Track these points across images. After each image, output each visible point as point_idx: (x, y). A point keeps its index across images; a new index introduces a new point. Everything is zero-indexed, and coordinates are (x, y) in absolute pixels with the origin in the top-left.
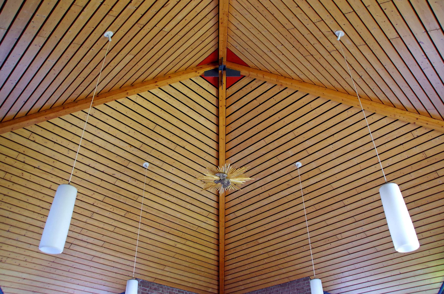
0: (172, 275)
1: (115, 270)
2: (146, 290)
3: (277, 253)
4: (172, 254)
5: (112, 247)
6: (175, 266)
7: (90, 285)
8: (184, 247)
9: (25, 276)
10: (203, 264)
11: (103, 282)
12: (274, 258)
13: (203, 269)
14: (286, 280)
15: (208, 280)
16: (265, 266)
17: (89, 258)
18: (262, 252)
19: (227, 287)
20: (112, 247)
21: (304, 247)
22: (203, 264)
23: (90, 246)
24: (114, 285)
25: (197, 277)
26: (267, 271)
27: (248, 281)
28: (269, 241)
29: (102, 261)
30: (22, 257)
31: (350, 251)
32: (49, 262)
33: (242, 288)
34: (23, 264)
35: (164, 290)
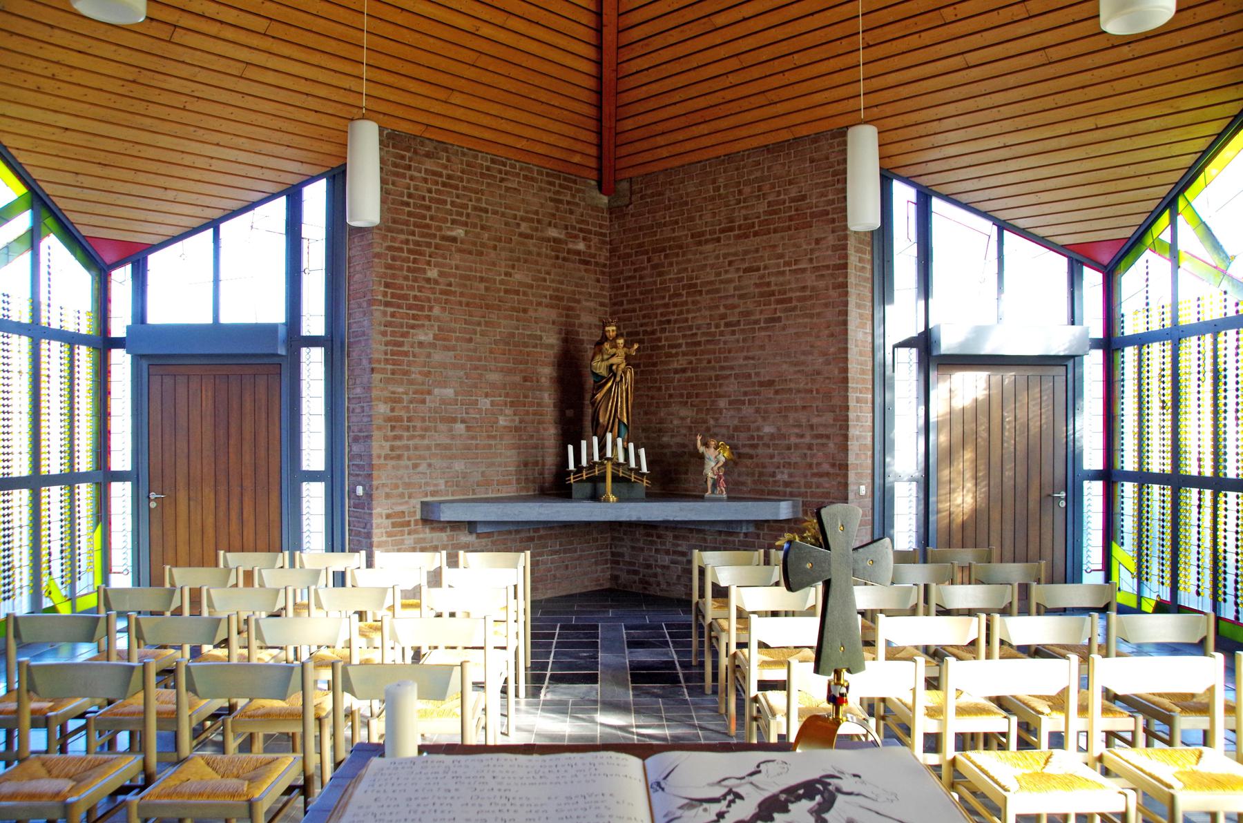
0: (473, 117)
1: (312, 103)
2: (403, 157)
3: (764, 58)
4: (469, 56)
5: (293, 35)
6: (481, 91)
7: (247, 144)
8: (502, 36)
9: (64, 121)
10: (555, 86)
11: (286, 139)
12: (756, 72)
13: (556, 101)
14: (785, 135)
15: (571, 131)
16: (729, 95)
17: (235, 68)
18: (722, 52)
19: (623, 151)
20: (293, 35)
21: (844, 41)
22: (555, 86)
23: (229, 33)
24: (316, 146)
25: (540, 122)
26: (735, 107)
27: (680, 136)
28: (745, 19)
29: (270, 78)
30: (37, 67)
31: (973, 58)
32: (121, 83)
33: (664, 153)
34: (48, 85)
35: (453, 158)
